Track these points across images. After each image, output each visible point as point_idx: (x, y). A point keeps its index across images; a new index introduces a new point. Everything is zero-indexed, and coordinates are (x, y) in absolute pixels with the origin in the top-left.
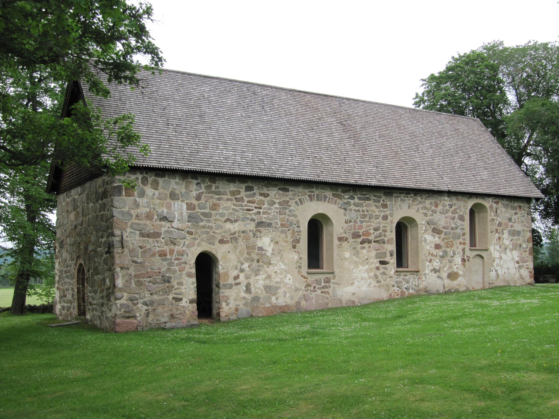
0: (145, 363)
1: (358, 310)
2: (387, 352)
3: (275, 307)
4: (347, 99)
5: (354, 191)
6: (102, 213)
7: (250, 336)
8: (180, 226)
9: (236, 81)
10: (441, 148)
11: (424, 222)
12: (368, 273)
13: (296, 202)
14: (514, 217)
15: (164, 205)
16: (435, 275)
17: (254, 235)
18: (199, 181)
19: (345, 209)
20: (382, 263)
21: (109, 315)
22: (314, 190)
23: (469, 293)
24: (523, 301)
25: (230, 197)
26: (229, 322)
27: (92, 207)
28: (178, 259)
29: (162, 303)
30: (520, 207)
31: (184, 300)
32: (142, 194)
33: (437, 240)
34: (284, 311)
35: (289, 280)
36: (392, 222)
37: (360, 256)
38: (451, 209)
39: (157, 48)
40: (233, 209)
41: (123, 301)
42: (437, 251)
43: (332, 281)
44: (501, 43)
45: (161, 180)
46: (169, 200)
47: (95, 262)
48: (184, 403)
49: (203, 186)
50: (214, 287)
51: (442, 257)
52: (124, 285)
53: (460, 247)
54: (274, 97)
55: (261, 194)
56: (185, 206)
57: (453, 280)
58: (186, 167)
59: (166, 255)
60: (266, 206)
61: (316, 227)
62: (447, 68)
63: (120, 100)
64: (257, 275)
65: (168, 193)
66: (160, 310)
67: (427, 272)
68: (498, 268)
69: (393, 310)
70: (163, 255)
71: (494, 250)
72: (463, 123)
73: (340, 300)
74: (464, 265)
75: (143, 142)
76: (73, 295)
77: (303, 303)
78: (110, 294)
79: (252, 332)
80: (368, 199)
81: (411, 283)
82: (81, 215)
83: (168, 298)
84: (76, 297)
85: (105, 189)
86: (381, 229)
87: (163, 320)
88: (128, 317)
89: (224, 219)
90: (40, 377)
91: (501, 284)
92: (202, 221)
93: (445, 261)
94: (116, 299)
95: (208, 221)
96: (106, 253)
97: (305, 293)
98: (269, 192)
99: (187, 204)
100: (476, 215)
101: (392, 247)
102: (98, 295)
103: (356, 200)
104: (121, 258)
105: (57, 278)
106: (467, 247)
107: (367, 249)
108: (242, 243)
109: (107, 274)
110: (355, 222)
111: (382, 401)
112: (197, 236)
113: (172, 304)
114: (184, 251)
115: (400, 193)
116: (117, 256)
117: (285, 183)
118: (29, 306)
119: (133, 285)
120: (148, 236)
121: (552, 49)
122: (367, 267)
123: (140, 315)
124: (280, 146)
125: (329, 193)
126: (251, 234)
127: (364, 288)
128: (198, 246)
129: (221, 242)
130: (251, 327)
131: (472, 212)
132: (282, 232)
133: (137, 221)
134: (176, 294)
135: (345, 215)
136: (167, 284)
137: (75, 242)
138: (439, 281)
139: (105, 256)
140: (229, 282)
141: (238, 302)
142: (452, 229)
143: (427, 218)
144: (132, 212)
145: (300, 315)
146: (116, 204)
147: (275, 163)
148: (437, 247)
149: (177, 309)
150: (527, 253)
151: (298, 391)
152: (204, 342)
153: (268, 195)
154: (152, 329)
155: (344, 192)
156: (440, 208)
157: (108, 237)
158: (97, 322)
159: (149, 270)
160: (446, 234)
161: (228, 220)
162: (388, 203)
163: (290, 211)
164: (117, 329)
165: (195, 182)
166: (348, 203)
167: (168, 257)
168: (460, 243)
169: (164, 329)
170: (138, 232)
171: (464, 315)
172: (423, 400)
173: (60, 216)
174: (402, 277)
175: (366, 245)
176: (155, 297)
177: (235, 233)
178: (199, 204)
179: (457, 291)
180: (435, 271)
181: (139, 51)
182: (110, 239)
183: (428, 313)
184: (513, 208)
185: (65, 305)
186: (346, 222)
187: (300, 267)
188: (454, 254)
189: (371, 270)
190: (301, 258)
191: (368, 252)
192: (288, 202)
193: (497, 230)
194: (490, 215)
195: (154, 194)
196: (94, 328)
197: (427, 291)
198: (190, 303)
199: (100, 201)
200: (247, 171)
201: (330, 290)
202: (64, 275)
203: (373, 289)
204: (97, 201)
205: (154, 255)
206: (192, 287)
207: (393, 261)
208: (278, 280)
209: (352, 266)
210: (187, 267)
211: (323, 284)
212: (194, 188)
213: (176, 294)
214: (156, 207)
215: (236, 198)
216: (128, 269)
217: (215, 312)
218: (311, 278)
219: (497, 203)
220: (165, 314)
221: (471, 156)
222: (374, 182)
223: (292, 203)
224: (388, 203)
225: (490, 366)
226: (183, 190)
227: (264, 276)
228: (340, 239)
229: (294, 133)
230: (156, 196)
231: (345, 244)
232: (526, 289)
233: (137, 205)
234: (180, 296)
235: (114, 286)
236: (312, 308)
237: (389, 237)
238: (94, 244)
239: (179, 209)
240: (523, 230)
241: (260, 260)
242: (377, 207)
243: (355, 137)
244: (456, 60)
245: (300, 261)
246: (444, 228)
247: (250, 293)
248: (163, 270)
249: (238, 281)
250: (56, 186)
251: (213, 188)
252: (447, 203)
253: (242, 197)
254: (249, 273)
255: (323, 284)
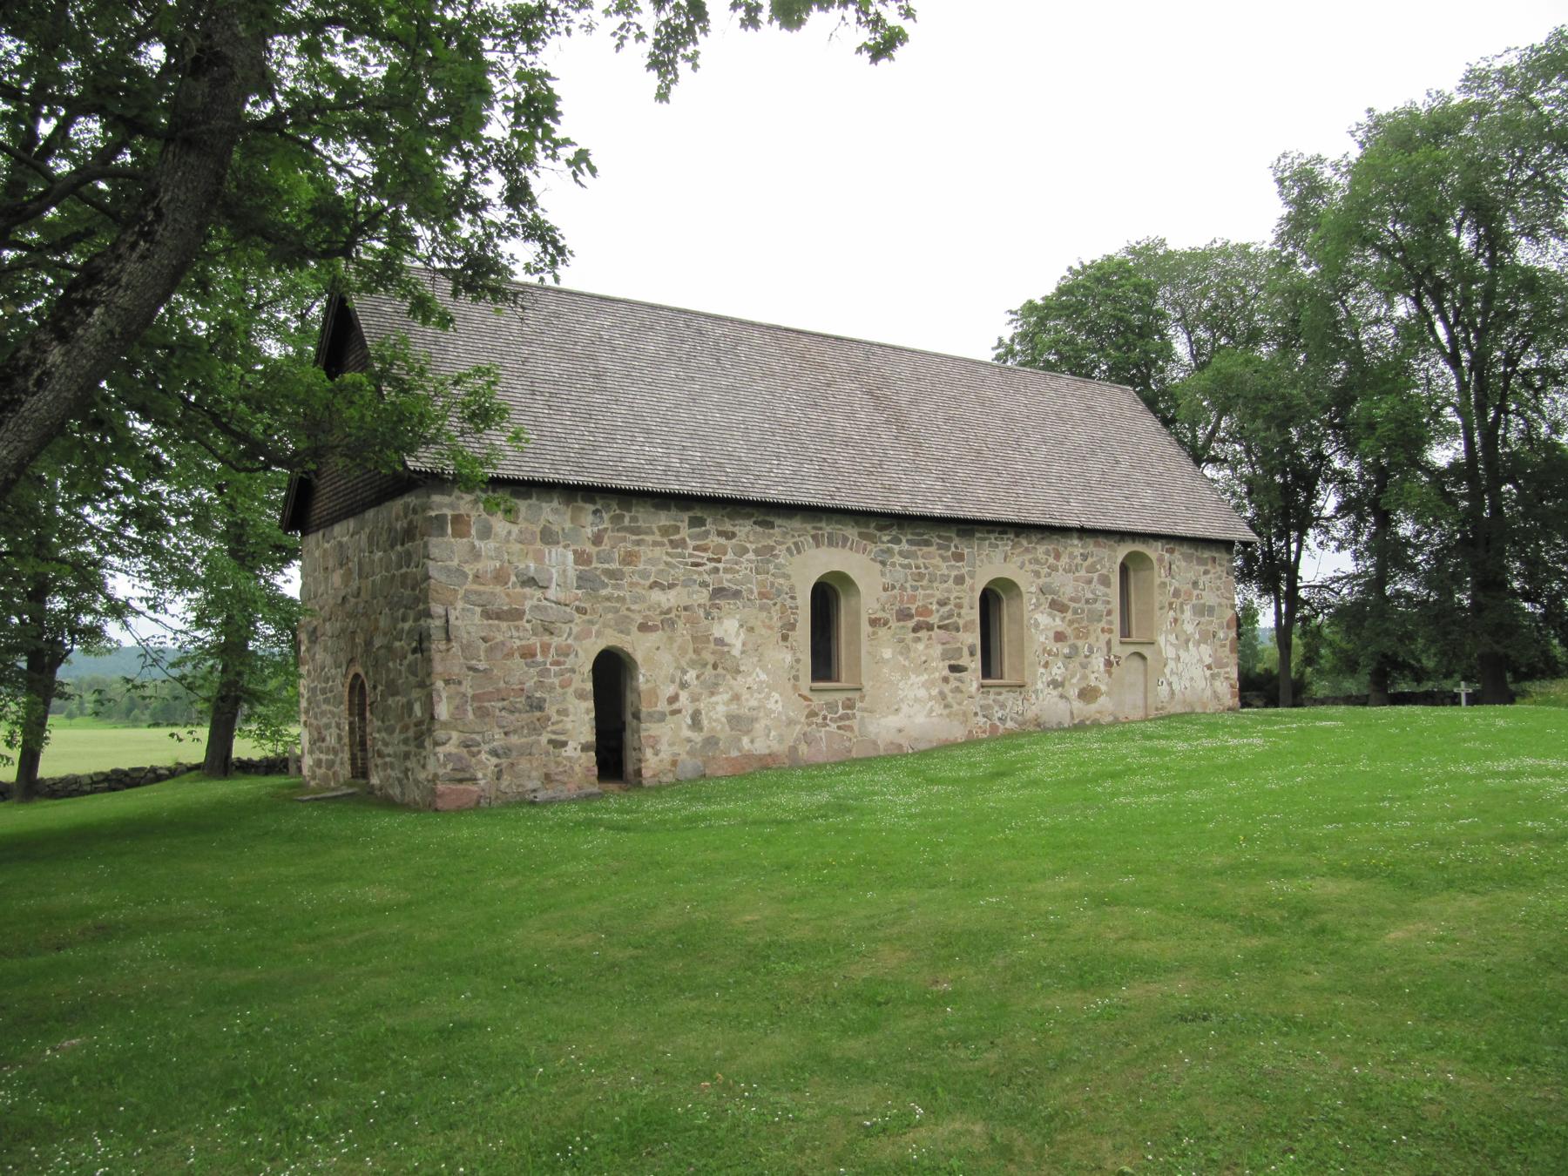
0: (517, 872)
1: (918, 761)
2: (1013, 844)
3: (749, 757)
4: (881, 346)
5: (900, 527)
6: (404, 570)
7: (713, 814)
8: (562, 597)
9: (662, 308)
10: (1062, 443)
11: (1033, 589)
12: (928, 689)
13: (788, 549)
14: (1203, 579)
15: (531, 555)
16: (1055, 693)
17: (708, 614)
18: (599, 507)
19: (883, 563)
20: (953, 669)
21: (422, 776)
22: (823, 524)
23: (1118, 728)
24: (1232, 742)
25: (659, 539)
26: (659, 788)
27: (381, 559)
28: (557, 663)
29: (527, 751)
30: (1214, 559)
31: (571, 744)
32: (486, 533)
33: (1058, 623)
34: (766, 763)
35: (775, 703)
36: (972, 589)
37: (912, 655)
38: (1086, 564)
39: (552, 229)
40: (667, 563)
41: (450, 748)
42: (1059, 645)
43: (858, 704)
44: (1162, 242)
45: (522, 505)
46: (539, 545)
47: (388, 670)
48: (631, 951)
49: (606, 516)
50: (629, 718)
51: (1068, 657)
52: (452, 715)
53: (1101, 639)
54: (737, 342)
55: (720, 534)
56: (571, 557)
57: (1089, 702)
58: (573, 479)
59: (534, 655)
60: (730, 556)
61: (827, 599)
62: (1059, 289)
63: (436, 343)
64: (712, 694)
65: (538, 530)
66: (524, 764)
67: (1040, 686)
68: (1174, 679)
69: (983, 761)
70: (528, 654)
71: (1165, 643)
72: (1102, 395)
73: (875, 743)
74: (1110, 674)
75: (516, 419)
76: (340, 738)
77: (803, 749)
78: (423, 734)
79: (716, 808)
80: (927, 543)
81: (1010, 709)
82: (356, 575)
83: (538, 742)
84: (346, 740)
85: (411, 522)
86: (953, 601)
87: (530, 785)
88: (461, 781)
89: (648, 583)
90: (310, 901)
91: (1179, 709)
92: (605, 586)
93: (1074, 664)
94: (436, 744)
95: (617, 587)
96: (414, 651)
97: (806, 729)
98: (736, 529)
99: (575, 552)
100: (1132, 574)
101: (974, 638)
102: (397, 736)
103: (905, 546)
104: (446, 661)
105: (304, 704)
106: (1116, 637)
107: (925, 641)
108: (683, 630)
109: (416, 693)
110: (903, 588)
111: (1051, 941)
112: (595, 617)
113: (547, 754)
114: (569, 646)
115: (989, 532)
116: (437, 657)
117: (767, 511)
118: (239, 759)
119: (471, 716)
120: (499, 616)
121: (1256, 256)
122: (926, 677)
123: (485, 776)
124: (755, 437)
125: (851, 532)
126: (701, 613)
127: (920, 719)
128: (597, 636)
129: (644, 628)
130: (709, 798)
131: (1124, 569)
132: (762, 608)
133: (475, 587)
134: (554, 732)
135: (883, 574)
136: (538, 714)
137: (343, 630)
138: (1062, 704)
139: (410, 657)
140: (659, 708)
141: (676, 749)
142: (1087, 601)
143: (1041, 581)
144: (466, 568)
145: (799, 772)
146: (434, 552)
147: (747, 471)
148: (1059, 637)
149: (558, 764)
150: (1227, 649)
151: (866, 923)
152: (626, 829)
153: (734, 535)
154: (507, 804)
155: (880, 528)
156: (1064, 560)
157: (417, 620)
158: (395, 792)
159: (502, 684)
160: (1075, 612)
161: (655, 584)
162: (966, 551)
163: (776, 567)
164: (440, 804)
165: (591, 507)
166: (889, 551)
167: (539, 658)
168: (1103, 631)
169: (533, 803)
170: (478, 610)
171: (1128, 770)
172: (1133, 937)
173: (310, 579)
174: (992, 696)
175: (923, 634)
176: (514, 739)
177: (669, 611)
178: (598, 553)
179: (1096, 724)
180: (1055, 684)
181: (514, 234)
182: (422, 622)
183: (1055, 767)
184: (1201, 561)
185: (323, 757)
186: (885, 589)
187: (796, 678)
188: (1091, 650)
189: (932, 683)
190: (798, 661)
191: (927, 647)
192: (773, 548)
193: (1171, 604)
194: (1159, 574)
195: (509, 533)
196: (389, 804)
197: (1039, 725)
198: (583, 750)
199: (399, 548)
200: (693, 486)
201: (855, 723)
202: (320, 698)
203: (935, 720)
204: (392, 546)
205: (510, 655)
206: (587, 718)
207: (975, 664)
208: (753, 703)
209: (896, 676)
210: (576, 677)
211: (841, 711)
212: (589, 521)
213: (554, 732)
214: (514, 559)
215: (671, 542)
216: (460, 683)
217: (630, 767)
218: (818, 701)
219: (1171, 551)
220: (534, 774)
221: (1114, 459)
222: (938, 510)
223: (780, 550)
224: (966, 551)
225: (1234, 868)
226: (568, 525)
227: (726, 697)
228: (874, 622)
229: (781, 413)
230: (514, 536)
231: (882, 632)
232: (1229, 718)
233: (476, 555)
234: (563, 738)
235: (432, 717)
236: (821, 760)
237: (968, 618)
238: (385, 634)
239: (560, 562)
240: (1220, 605)
241: (717, 663)
242: (944, 559)
243: (899, 422)
244: (1077, 273)
245: (797, 666)
246: (1072, 599)
247: (701, 729)
248: (530, 684)
249: (676, 706)
250: (300, 513)
251: (627, 520)
252: (1077, 551)
253: (683, 540)
254: (698, 690)
255: (841, 711)
